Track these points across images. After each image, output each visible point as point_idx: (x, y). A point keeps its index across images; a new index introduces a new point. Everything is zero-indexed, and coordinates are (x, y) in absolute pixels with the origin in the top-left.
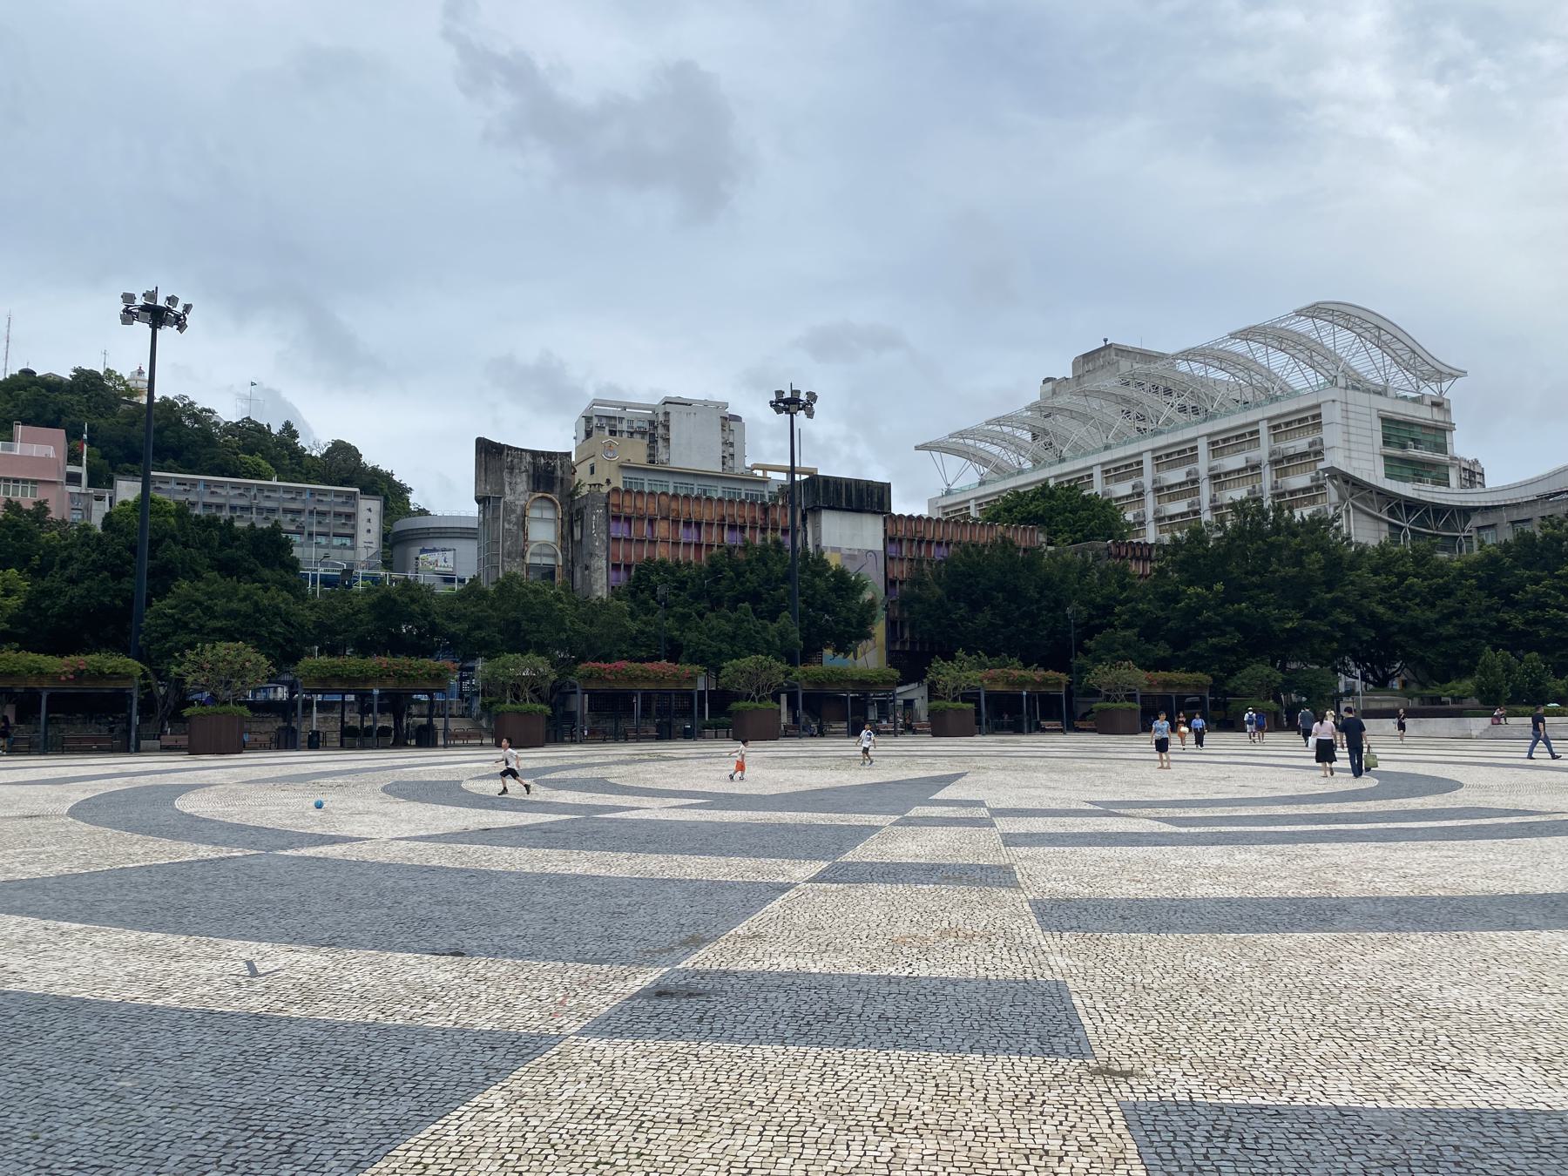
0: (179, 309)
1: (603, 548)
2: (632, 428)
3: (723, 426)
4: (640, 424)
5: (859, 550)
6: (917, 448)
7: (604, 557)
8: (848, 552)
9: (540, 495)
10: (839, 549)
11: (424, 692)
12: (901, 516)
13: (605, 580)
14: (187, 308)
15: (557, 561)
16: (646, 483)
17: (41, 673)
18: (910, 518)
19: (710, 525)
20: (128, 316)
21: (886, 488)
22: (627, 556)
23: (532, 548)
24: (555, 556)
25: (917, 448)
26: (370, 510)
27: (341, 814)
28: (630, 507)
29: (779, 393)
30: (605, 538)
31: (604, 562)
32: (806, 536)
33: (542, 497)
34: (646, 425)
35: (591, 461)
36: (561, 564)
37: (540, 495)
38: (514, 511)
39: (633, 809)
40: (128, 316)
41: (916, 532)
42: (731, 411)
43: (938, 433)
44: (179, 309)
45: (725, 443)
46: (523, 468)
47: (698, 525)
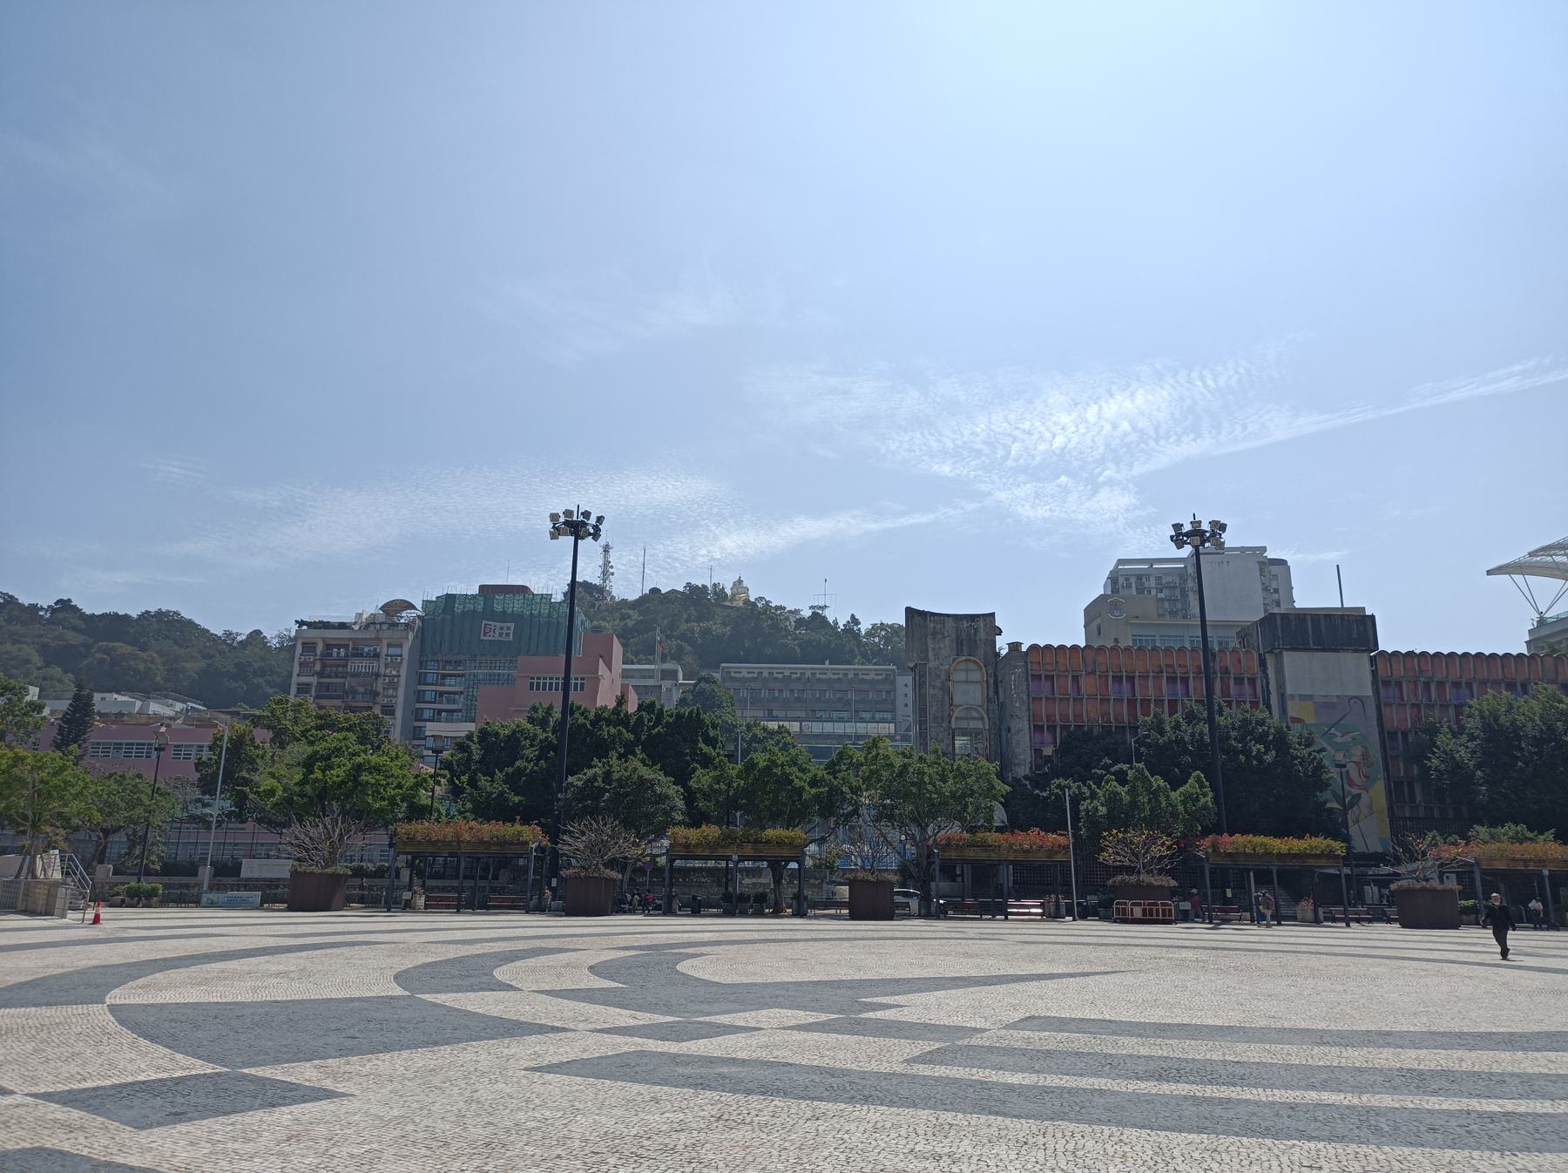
0: (592, 520)
1: (1024, 708)
2: (1161, 584)
3: (1261, 572)
4: (1170, 579)
5: (1338, 697)
6: (1489, 573)
7: (1026, 719)
8: (1324, 700)
9: (964, 658)
10: (1310, 697)
11: (962, 871)
12: (1396, 653)
13: (1028, 744)
14: (600, 519)
15: (984, 724)
16: (1157, 638)
17: (1268, 854)
18: (1411, 654)
19: (1145, 677)
20: (556, 533)
21: (1370, 623)
22: (1050, 717)
23: (957, 713)
24: (982, 719)
25: (1489, 573)
26: (906, 685)
27: (225, 1010)
28: (1051, 664)
29: (1177, 527)
30: (1025, 698)
31: (1026, 723)
32: (1268, 683)
33: (966, 660)
34: (1177, 581)
35: (1098, 621)
36: (987, 728)
37: (964, 658)
38: (938, 676)
39: (799, 1028)
40: (556, 533)
41: (1421, 671)
42: (1270, 554)
43: (1518, 553)
44: (592, 520)
45: (1265, 589)
46: (946, 634)
47: (1050, 678)
